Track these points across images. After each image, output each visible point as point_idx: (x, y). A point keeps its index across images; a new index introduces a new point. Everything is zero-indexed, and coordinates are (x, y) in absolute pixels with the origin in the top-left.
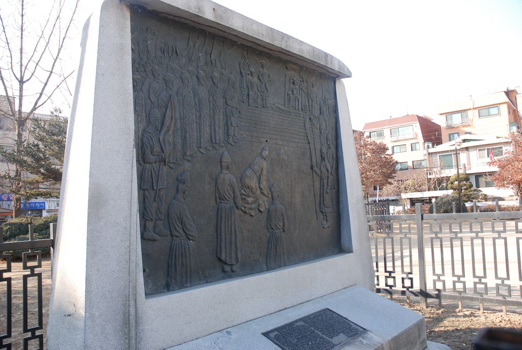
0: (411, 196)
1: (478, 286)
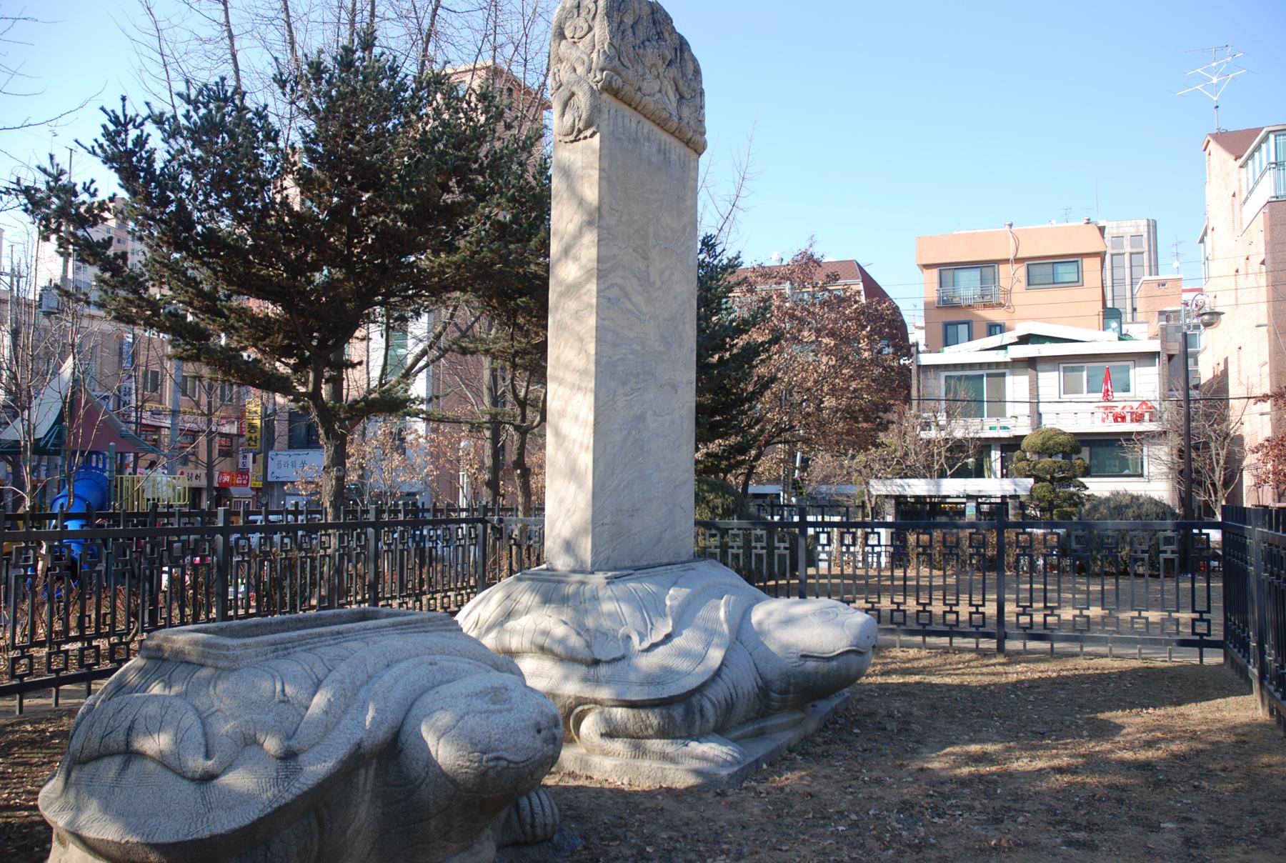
0: (900, 489)
1: (974, 616)
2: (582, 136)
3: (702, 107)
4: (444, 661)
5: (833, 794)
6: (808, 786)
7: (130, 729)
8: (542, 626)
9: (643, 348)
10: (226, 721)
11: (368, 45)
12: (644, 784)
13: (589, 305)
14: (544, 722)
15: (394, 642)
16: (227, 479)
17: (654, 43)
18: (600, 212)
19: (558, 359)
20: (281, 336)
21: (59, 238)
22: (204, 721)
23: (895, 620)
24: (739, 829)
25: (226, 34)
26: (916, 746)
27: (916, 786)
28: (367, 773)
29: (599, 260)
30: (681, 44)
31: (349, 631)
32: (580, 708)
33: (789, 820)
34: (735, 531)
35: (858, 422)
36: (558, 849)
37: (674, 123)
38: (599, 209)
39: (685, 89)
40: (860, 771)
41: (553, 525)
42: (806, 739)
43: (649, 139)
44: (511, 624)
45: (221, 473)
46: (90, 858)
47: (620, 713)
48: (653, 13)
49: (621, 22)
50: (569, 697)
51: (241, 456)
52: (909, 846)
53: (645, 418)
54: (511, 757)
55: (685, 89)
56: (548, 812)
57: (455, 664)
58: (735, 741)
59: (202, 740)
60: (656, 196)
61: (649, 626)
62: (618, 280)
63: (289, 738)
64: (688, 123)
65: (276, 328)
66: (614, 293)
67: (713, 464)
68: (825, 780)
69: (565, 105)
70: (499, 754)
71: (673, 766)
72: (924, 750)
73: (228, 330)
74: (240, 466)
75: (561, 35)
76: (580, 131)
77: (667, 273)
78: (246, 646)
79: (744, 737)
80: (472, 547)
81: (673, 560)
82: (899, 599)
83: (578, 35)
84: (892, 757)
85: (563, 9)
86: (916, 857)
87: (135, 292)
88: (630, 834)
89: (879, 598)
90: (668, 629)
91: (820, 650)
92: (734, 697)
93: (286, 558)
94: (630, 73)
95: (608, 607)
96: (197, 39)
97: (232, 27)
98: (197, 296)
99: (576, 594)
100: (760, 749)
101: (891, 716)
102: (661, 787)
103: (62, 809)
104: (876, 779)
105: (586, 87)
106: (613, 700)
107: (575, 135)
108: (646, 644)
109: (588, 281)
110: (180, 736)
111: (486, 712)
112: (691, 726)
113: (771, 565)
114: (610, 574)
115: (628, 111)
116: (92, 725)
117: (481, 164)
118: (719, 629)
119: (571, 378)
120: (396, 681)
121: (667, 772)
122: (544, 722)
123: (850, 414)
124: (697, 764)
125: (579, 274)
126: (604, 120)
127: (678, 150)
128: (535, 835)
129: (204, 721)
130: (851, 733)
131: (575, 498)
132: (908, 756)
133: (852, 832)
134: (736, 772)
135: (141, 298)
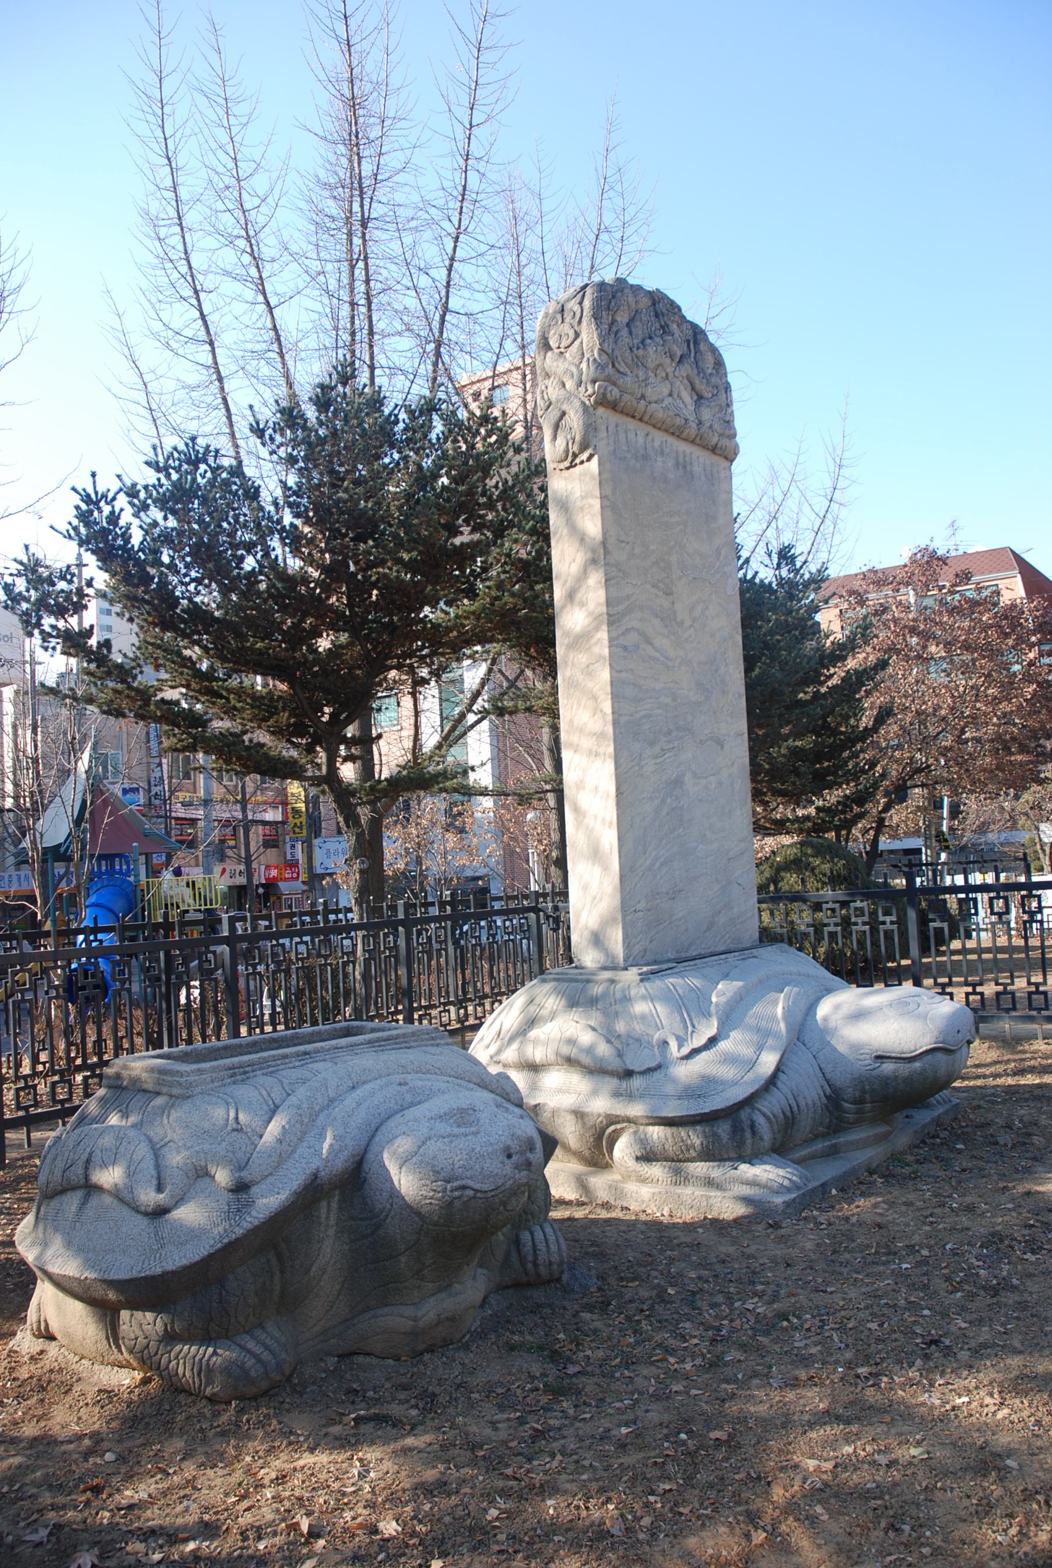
2: (578, 461)
3: (729, 405)
4: (416, 1081)
5: (907, 1225)
6: (881, 1215)
7: (88, 1162)
8: (568, 1034)
9: (674, 700)
10: (178, 1152)
11: (346, 376)
12: (688, 1215)
13: (601, 657)
14: (515, 1146)
15: (367, 1061)
16: (274, 873)
17: (658, 340)
18: (605, 547)
19: (571, 721)
20: (287, 714)
21: (42, 632)
22: (157, 1151)
23: (1034, 1005)
24: (782, 1267)
25: (215, 377)
26: (1030, 1163)
27: (1014, 1214)
28: (329, 1205)
29: (608, 603)
30: (695, 334)
31: (317, 1051)
32: (612, 1128)
33: (847, 1256)
34: (830, 905)
35: (1012, 754)
36: (567, 1291)
37: (692, 430)
38: (604, 543)
39: (703, 387)
40: (950, 1196)
41: (578, 916)
42: (895, 1158)
43: (662, 453)
44: (533, 1033)
45: (268, 867)
46: (61, 1295)
47: (656, 1133)
48: (654, 304)
49: (613, 322)
50: (599, 1115)
51: (288, 846)
52: (984, 1288)
53: (682, 783)
54: (477, 1186)
55: (703, 387)
56: (553, 1247)
57: (429, 1084)
58: (798, 1162)
59: (154, 1173)
60: (677, 519)
61: (690, 1029)
62: (636, 624)
63: (241, 1169)
64: (711, 427)
65: (281, 704)
66: (632, 638)
67: (823, 821)
68: (904, 1208)
69: (556, 427)
70: (464, 1182)
71: (719, 1193)
72: (1040, 1169)
73: (230, 712)
74: (289, 857)
75: (545, 346)
76: (575, 456)
77: (700, 607)
78: (200, 1071)
79: (812, 1157)
80: (525, 941)
81: (732, 947)
82: (1037, 978)
83: (564, 344)
84: (995, 1177)
85: (546, 315)
86: (989, 1301)
87: (123, 681)
88: (654, 1273)
89: (1012, 977)
90: (712, 1032)
91: (898, 1050)
92: (795, 1109)
93: (303, 967)
94: (629, 379)
95: (640, 1008)
96: (183, 388)
97: (221, 368)
98: (194, 676)
99: (605, 994)
100: (828, 1171)
101: (1009, 1126)
102: (705, 1218)
103: (33, 1244)
104: (967, 1207)
105: (577, 404)
106: (647, 1117)
107: (570, 459)
108: (685, 1051)
109: (597, 629)
110: (132, 1168)
111: (449, 1136)
112: (740, 1144)
113: (875, 944)
114: (645, 969)
115: (632, 424)
116: (55, 1159)
117: (490, 498)
118: (775, 1027)
119: (586, 743)
120: (359, 1104)
121: (712, 1201)
122: (515, 1146)
123: (1002, 744)
124: (746, 1191)
125: (587, 621)
126: (602, 440)
127: (701, 460)
128: (538, 1275)
129: (157, 1151)
130: (952, 1149)
131: (601, 883)
132: (1019, 1176)
133: (918, 1271)
134: (795, 1199)
135: (130, 687)
